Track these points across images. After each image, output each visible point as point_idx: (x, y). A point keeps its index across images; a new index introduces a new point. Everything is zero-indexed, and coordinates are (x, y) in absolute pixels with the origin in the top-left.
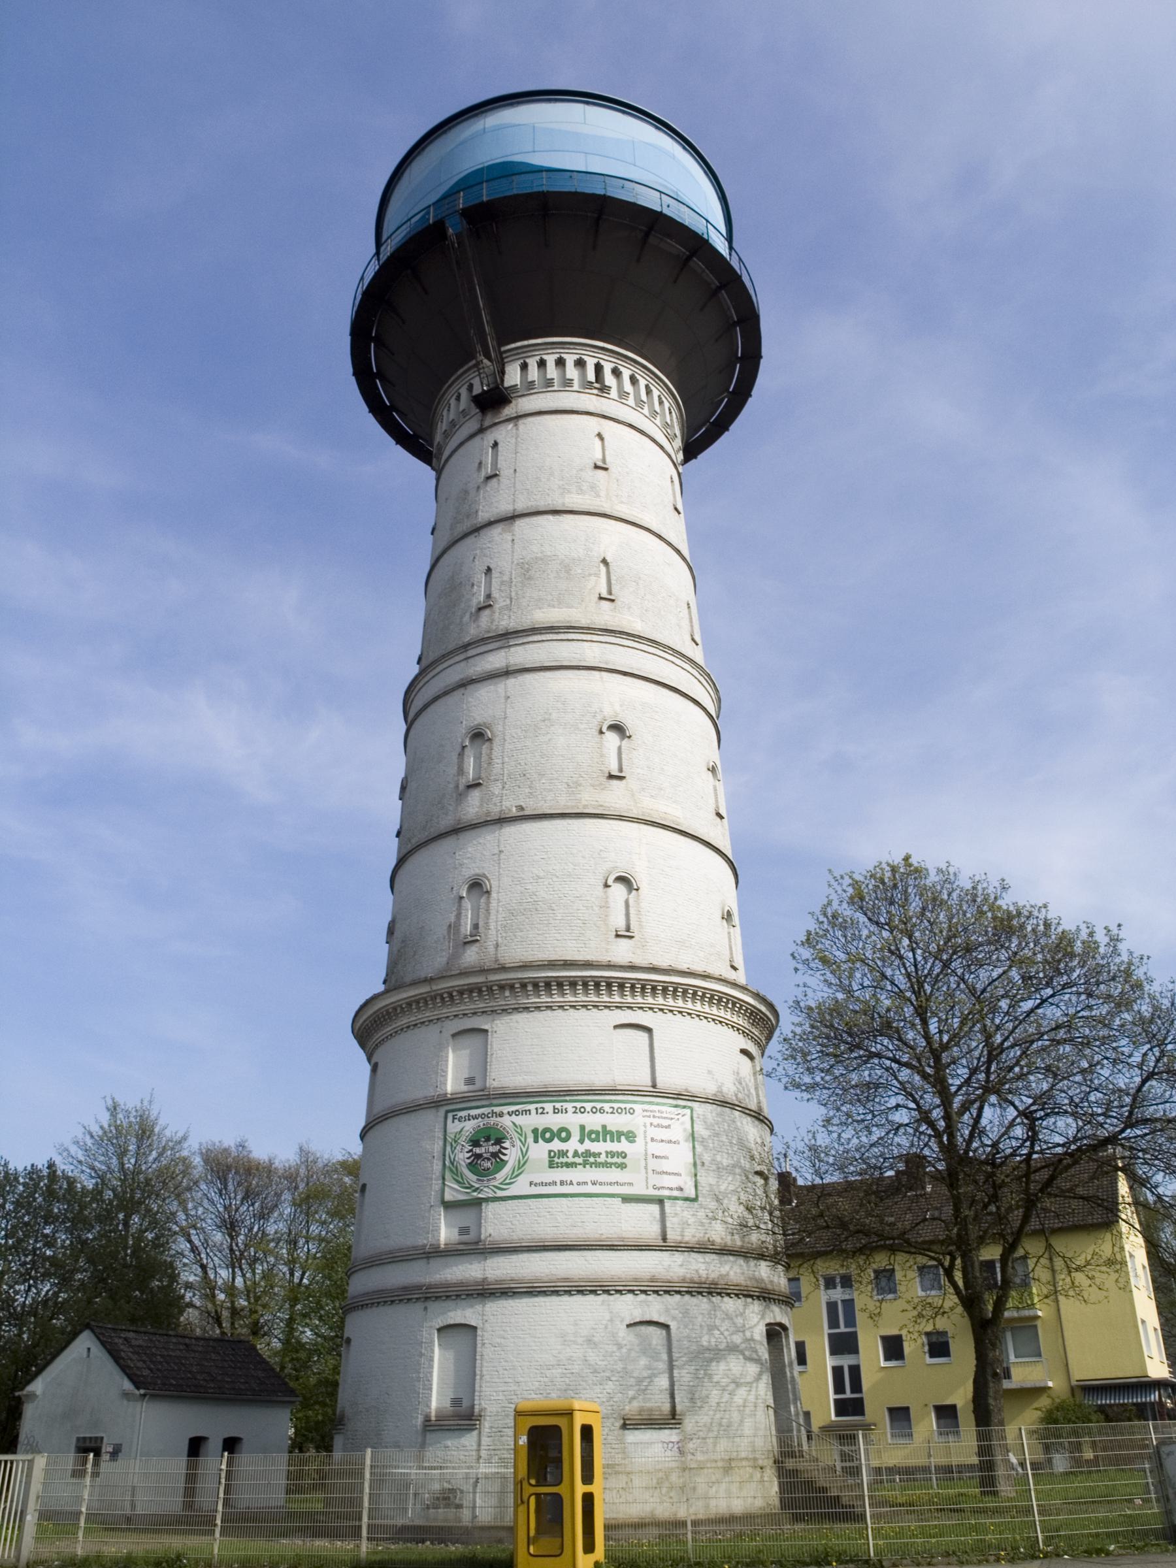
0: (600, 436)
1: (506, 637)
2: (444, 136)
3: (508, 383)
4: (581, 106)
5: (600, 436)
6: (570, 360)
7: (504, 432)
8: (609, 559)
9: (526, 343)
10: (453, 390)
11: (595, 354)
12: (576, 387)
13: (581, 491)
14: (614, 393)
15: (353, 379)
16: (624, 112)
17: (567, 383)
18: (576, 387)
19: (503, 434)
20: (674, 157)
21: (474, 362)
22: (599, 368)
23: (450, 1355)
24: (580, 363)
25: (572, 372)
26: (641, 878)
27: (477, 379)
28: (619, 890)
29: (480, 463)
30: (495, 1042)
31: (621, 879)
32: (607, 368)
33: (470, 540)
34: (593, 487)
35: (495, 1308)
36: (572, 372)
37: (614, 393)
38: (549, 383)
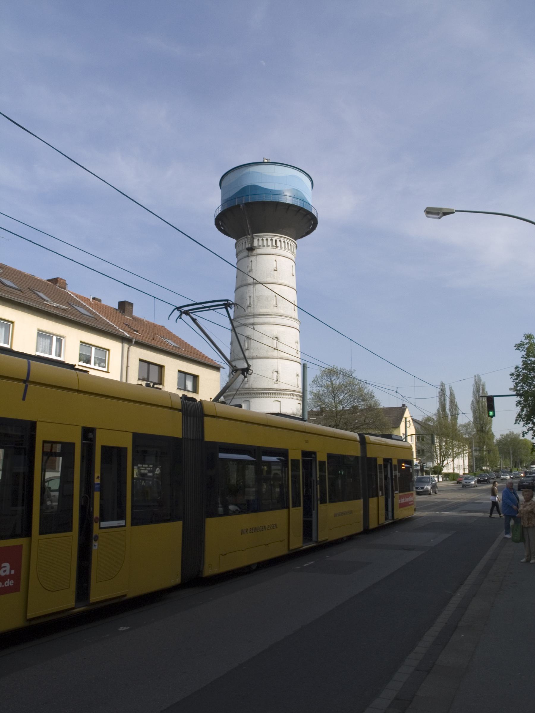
1: (254, 316)
3: (254, 245)
6: (269, 239)
11: (275, 237)
13: (271, 278)
14: (279, 248)
17: (268, 246)
19: (253, 258)
22: (276, 241)
23: (246, 405)
24: (272, 240)
25: (270, 243)
26: (280, 371)
28: (275, 374)
30: (251, 403)
31: (276, 338)
33: (246, 287)
34: (273, 276)
35: (255, 360)
36: (270, 243)
37: (279, 248)
38: (264, 246)
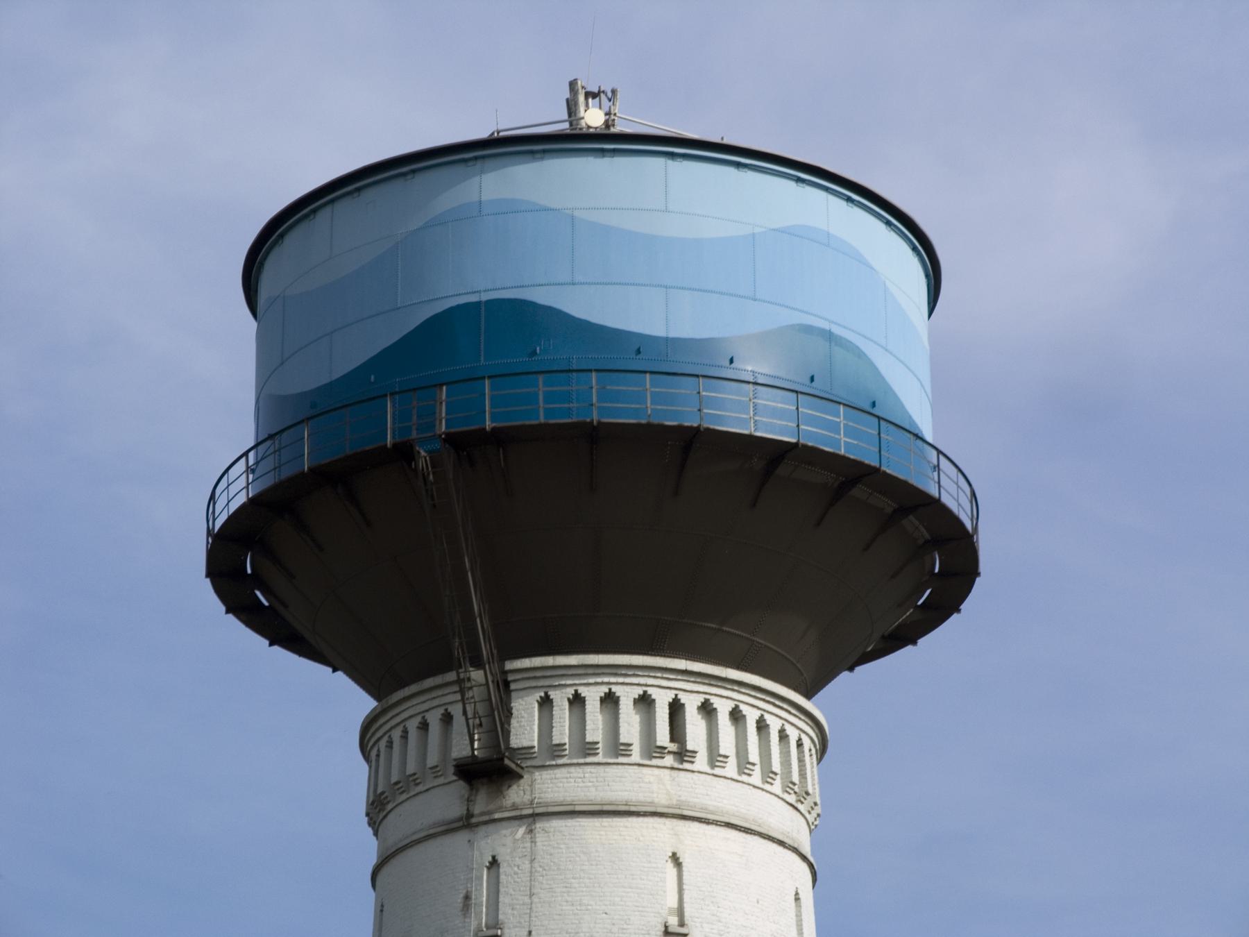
0: (675, 859)
2: (399, 183)
4: (659, 162)
5: (675, 859)
7: (509, 841)
8: (684, 859)
9: (549, 661)
10: (416, 706)
11: (669, 680)
12: (636, 756)
15: (208, 582)
16: (738, 165)
17: (619, 749)
18: (636, 756)
19: (505, 842)
20: (826, 241)
21: (451, 676)
22: (676, 709)
25: (630, 724)
27: (459, 706)
29: (467, 897)
32: (691, 704)
37: (701, 762)
38: (588, 749)
